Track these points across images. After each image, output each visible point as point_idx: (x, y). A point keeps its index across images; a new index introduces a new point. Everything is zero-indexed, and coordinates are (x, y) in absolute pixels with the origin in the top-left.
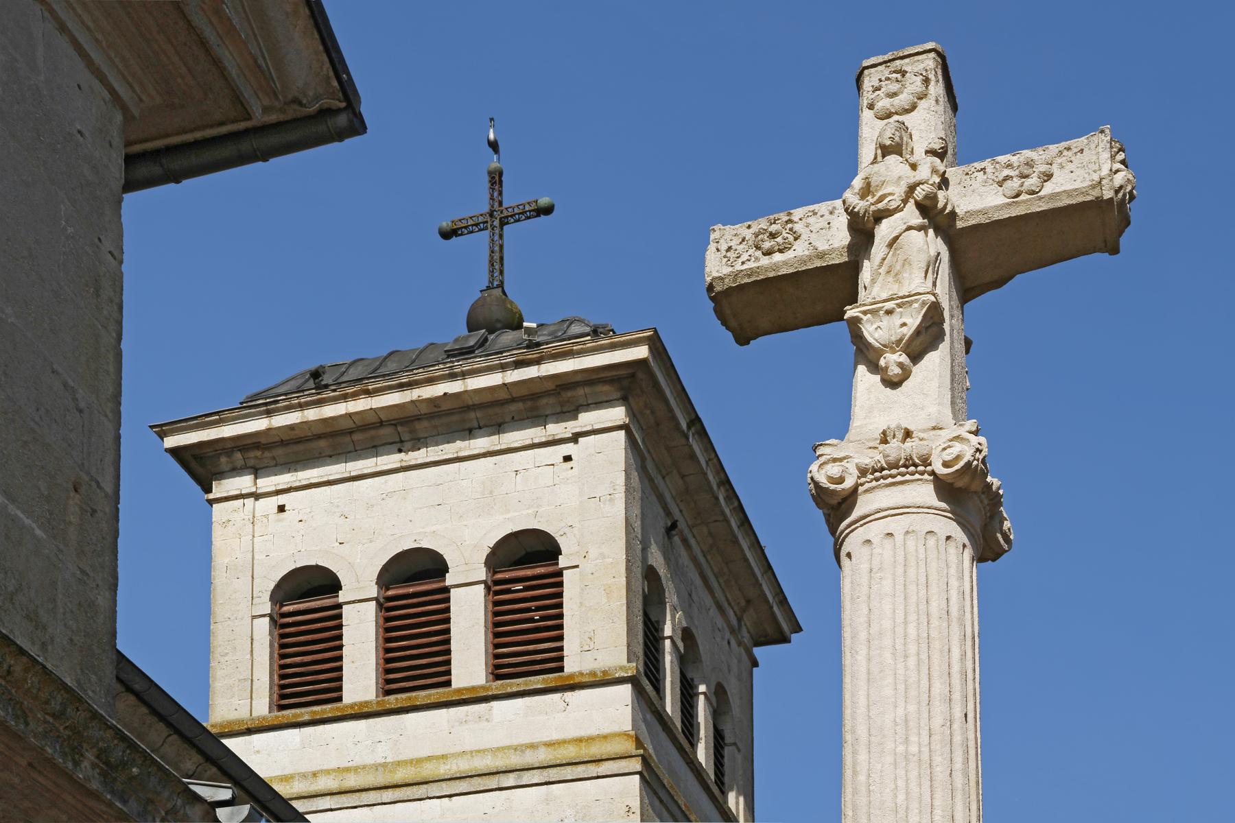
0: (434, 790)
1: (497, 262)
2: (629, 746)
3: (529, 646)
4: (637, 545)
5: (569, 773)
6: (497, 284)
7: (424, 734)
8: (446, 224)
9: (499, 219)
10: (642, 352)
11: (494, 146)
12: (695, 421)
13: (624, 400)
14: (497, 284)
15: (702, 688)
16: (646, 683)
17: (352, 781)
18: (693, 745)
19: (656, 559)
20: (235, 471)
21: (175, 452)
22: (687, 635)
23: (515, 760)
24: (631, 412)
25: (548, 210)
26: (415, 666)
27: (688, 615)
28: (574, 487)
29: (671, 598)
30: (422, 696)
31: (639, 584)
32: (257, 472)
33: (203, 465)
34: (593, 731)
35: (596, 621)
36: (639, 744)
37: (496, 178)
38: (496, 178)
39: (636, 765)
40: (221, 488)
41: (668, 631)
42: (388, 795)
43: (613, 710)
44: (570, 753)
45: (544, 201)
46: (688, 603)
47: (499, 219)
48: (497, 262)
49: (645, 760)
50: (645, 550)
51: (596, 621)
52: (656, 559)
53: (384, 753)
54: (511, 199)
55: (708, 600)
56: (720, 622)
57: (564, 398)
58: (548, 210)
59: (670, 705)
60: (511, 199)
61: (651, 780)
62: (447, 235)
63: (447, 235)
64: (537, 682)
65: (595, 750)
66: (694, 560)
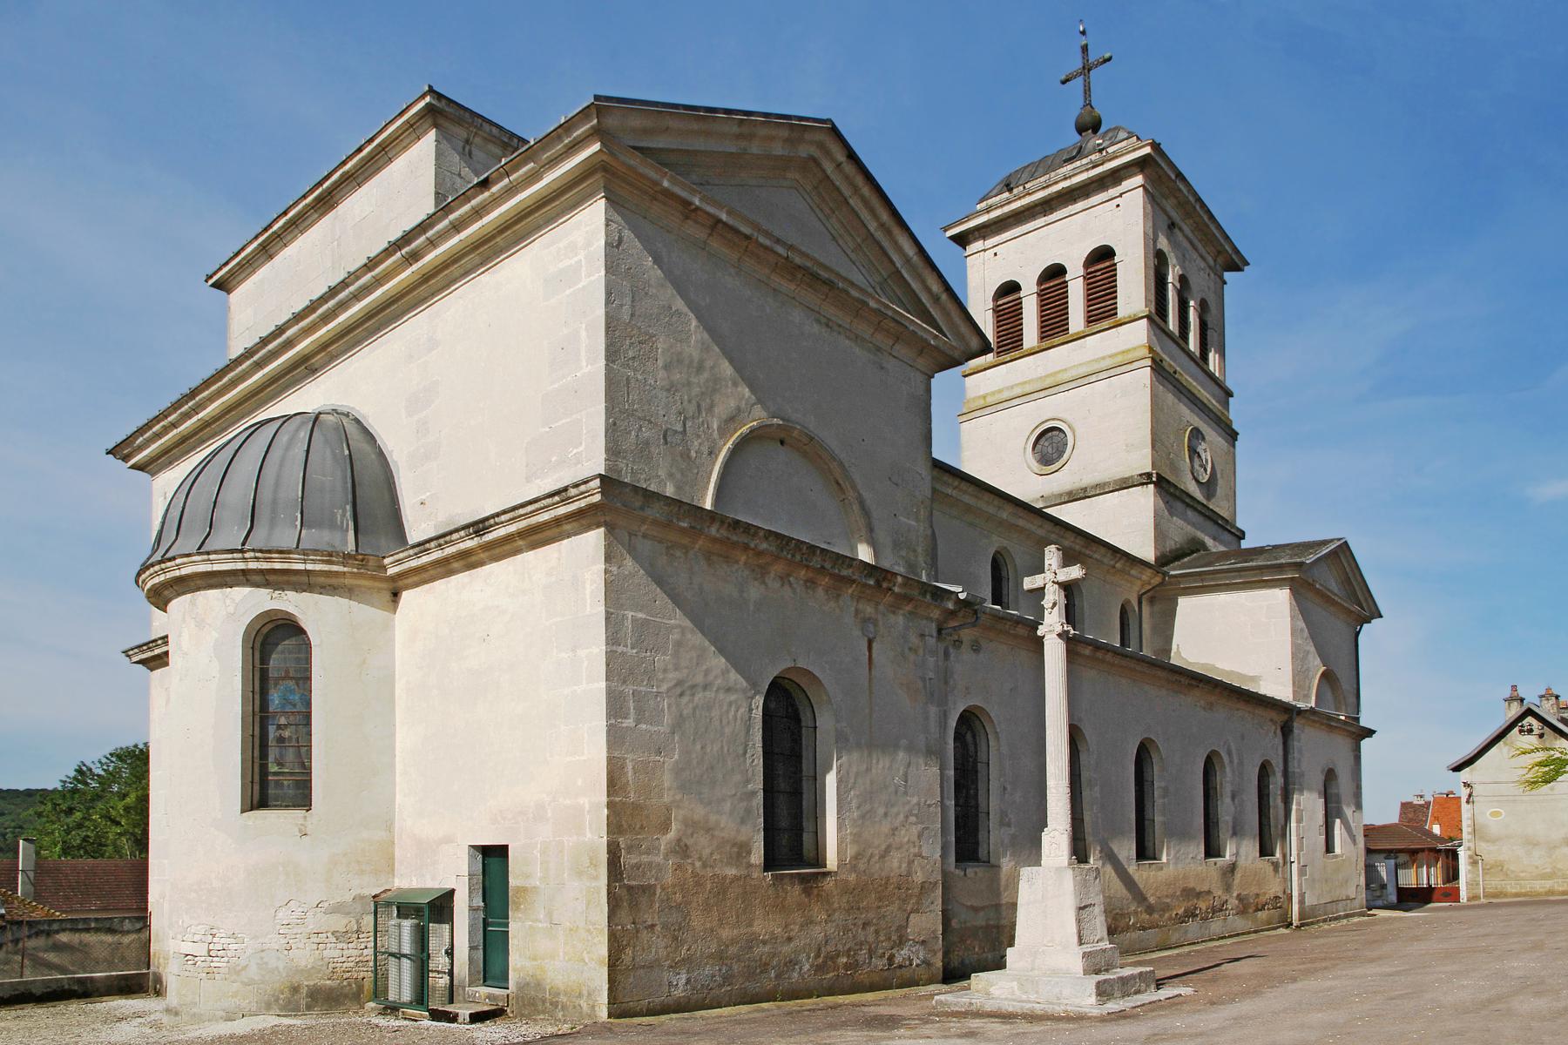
0: (1062, 388)
1: (1087, 91)
2: (1145, 352)
3: (1102, 309)
4: (1151, 240)
5: (1119, 370)
6: (1088, 104)
7: (1062, 358)
8: (1063, 77)
9: (1087, 69)
10: (1147, 150)
11: (1083, 33)
12: (1180, 175)
13: (1142, 171)
14: (1088, 104)
15: (1192, 303)
16: (1157, 318)
17: (1028, 389)
18: (1187, 342)
19: (1163, 244)
20: (976, 240)
21: (953, 238)
22: (1183, 279)
23: (1096, 367)
24: (1145, 177)
25: (1109, 59)
26: (1054, 326)
27: (1182, 267)
28: (1121, 220)
29: (1172, 259)
30: (1056, 341)
31: (1152, 262)
32: (984, 238)
33: (962, 240)
34: (1129, 346)
35: (1132, 292)
36: (1151, 349)
37: (1085, 49)
38: (1085, 49)
39: (1148, 362)
40: (972, 248)
41: (1170, 279)
42: (1042, 394)
43: (1136, 335)
44: (1119, 359)
45: (1107, 56)
46: (1182, 261)
47: (1087, 69)
48: (1087, 91)
49: (1153, 359)
50: (1155, 241)
51: (1132, 292)
52: (1163, 244)
53: (1041, 372)
54: (1092, 58)
55: (1195, 256)
56: (1203, 265)
57: (1115, 177)
58: (1109, 59)
59: (1173, 324)
60: (1092, 58)
61: (1158, 367)
62: (1064, 82)
63: (1064, 82)
64: (1105, 324)
65: (1130, 357)
66: (1187, 237)
